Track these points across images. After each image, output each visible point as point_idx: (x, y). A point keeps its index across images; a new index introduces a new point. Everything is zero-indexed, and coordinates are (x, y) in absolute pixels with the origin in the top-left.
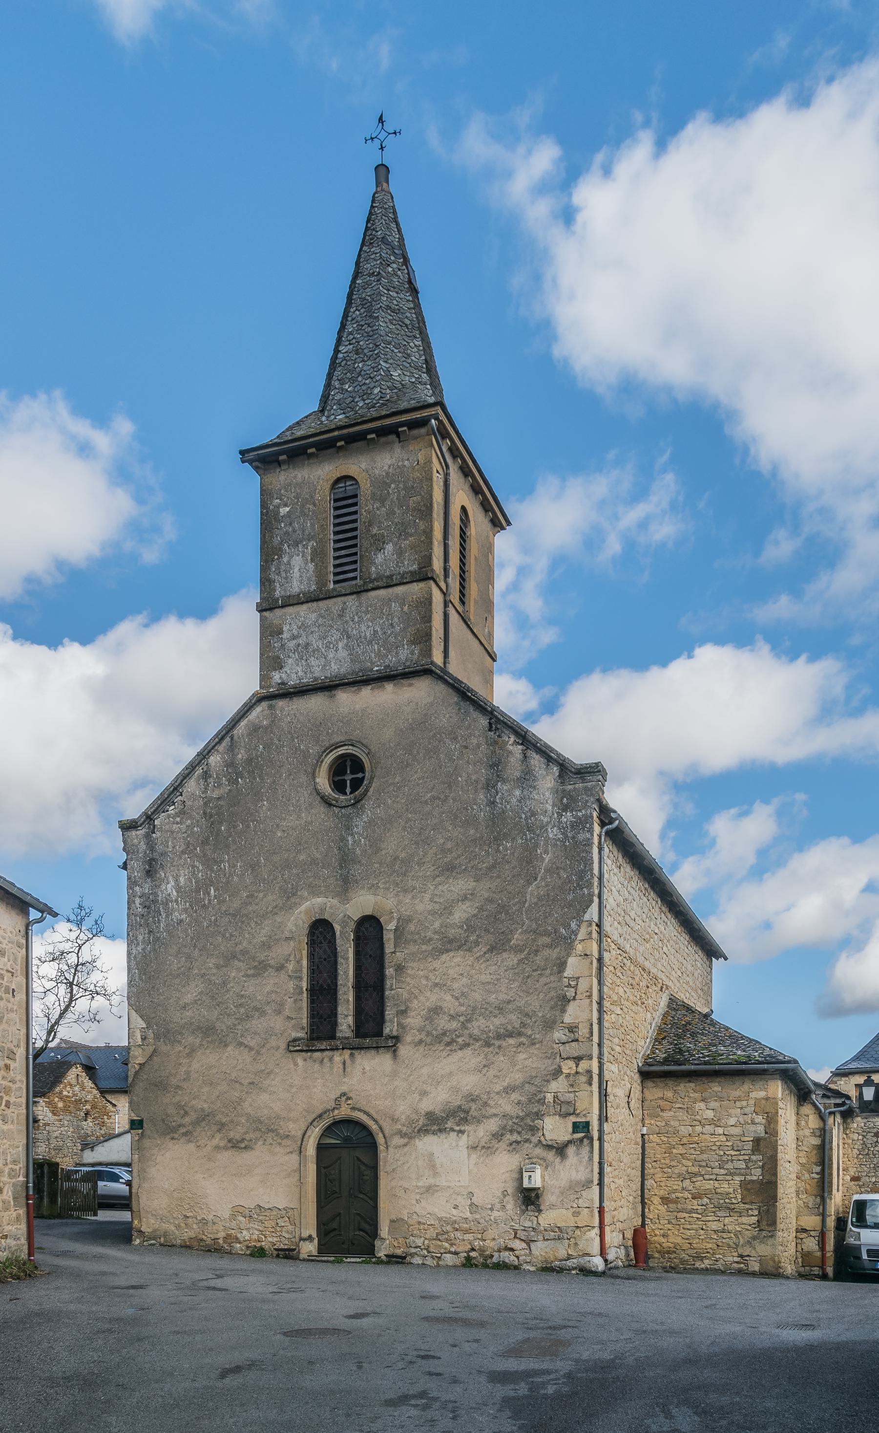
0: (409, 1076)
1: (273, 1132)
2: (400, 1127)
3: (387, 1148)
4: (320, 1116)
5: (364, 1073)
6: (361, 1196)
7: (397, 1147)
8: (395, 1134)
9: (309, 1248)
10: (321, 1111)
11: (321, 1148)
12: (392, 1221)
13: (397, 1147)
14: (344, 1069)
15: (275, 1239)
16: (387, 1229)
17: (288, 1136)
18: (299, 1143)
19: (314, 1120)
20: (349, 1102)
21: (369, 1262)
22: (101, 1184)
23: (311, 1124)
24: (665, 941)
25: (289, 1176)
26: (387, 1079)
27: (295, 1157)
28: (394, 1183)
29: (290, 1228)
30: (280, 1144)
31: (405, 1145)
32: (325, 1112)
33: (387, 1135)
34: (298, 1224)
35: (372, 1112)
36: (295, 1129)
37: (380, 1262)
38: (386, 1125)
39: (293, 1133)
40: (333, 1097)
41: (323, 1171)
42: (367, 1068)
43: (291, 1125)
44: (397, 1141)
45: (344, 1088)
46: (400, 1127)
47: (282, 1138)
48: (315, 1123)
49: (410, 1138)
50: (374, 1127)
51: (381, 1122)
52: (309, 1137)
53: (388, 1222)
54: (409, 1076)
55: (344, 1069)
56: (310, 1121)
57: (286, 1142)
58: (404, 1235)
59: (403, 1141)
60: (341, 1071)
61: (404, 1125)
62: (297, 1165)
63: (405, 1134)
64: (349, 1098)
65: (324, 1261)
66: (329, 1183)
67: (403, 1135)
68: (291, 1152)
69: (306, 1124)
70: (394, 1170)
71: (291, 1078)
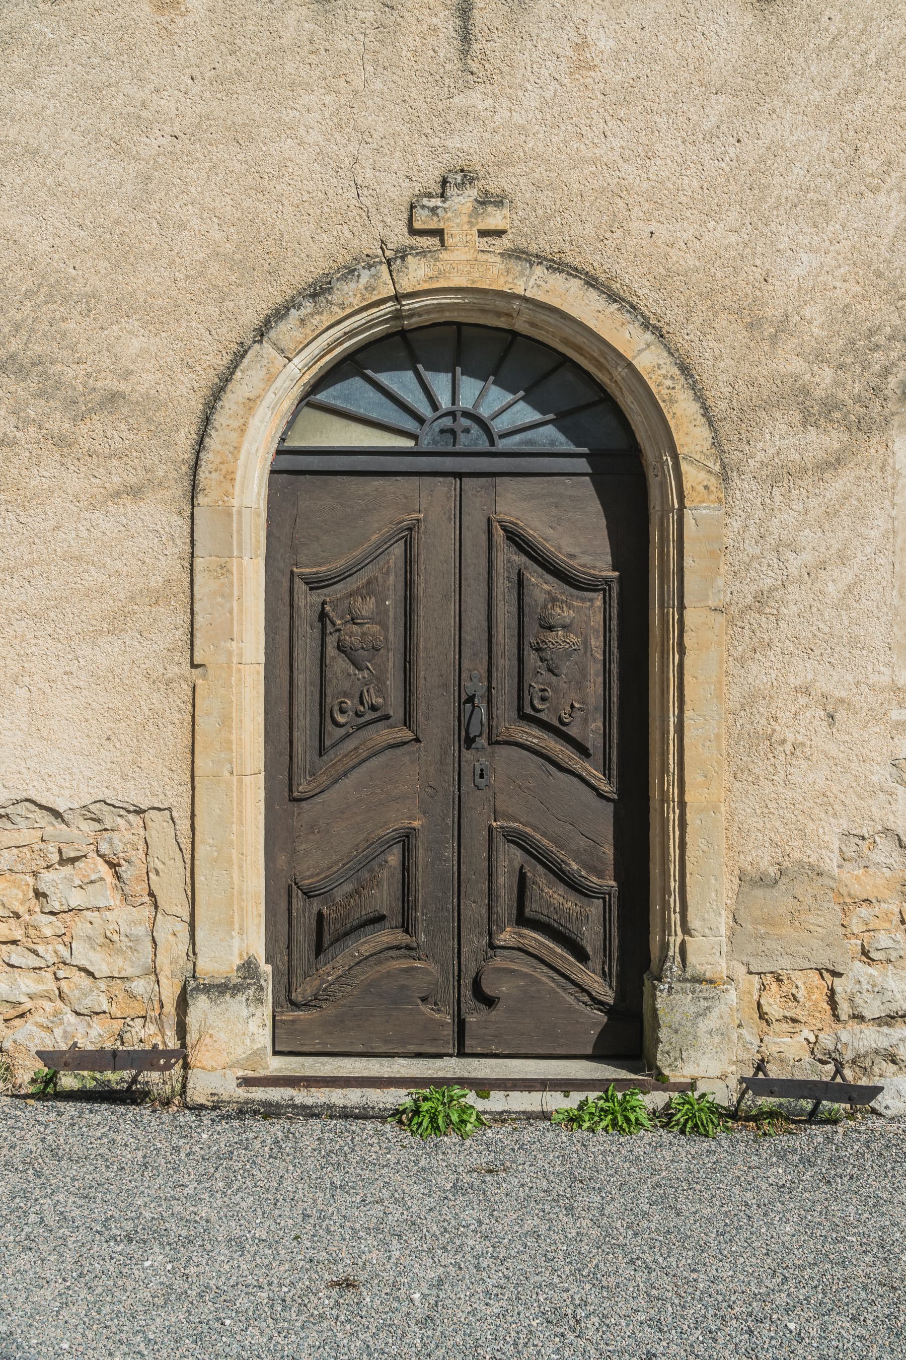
0: (846, 96)
1: (22, 372)
2: (797, 365)
3: (724, 477)
4: (319, 291)
5: (582, 66)
6: (533, 736)
7: (781, 475)
8: (768, 406)
9: (235, 1040)
10: (319, 267)
11: (294, 470)
12: (753, 882)
13: (781, 475)
14: (466, 37)
15: (27, 984)
16: (723, 923)
17: (114, 397)
18: (185, 439)
19: (280, 313)
20: (495, 219)
21: (621, 1122)
22: (588, 452)
23: (261, 333)
24: (642, 155)
25: (118, 622)
26: (720, 105)
27: (160, 515)
28: (759, 674)
29: (128, 919)
30: (62, 442)
31: (833, 463)
32: (350, 272)
33: (720, 408)
34: (174, 900)
35: (633, 278)
36: (162, 365)
37: (691, 1119)
38: (723, 358)
39: (147, 380)
40: (400, 192)
41: (307, 601)
42: (604, 43)
43: (134, 342)
44: (780, 439)
45: (465, 144)
46: (797, 365)
47: (80, 408)
48: (287, 331)
49: (862, 426)
50: (649, 359)
51: (685, 338)
52: (251, 404)
53: (728, 886)
54: (846, 96)
55: (466, 37)
56: (252, 318)
57: (92, 432)
58: (823, 958)
59: (821, 442)
60: (448, 50)
61: (820, 357)
62: (168, 566)
63: (830, 406)
64: (486, 201)
65: (346, 1114)
66: (339, 664)
67: (817, 411)
68: (135, 492)
69: (230, 335)
70: (761, 599)
71: (139, 80)
